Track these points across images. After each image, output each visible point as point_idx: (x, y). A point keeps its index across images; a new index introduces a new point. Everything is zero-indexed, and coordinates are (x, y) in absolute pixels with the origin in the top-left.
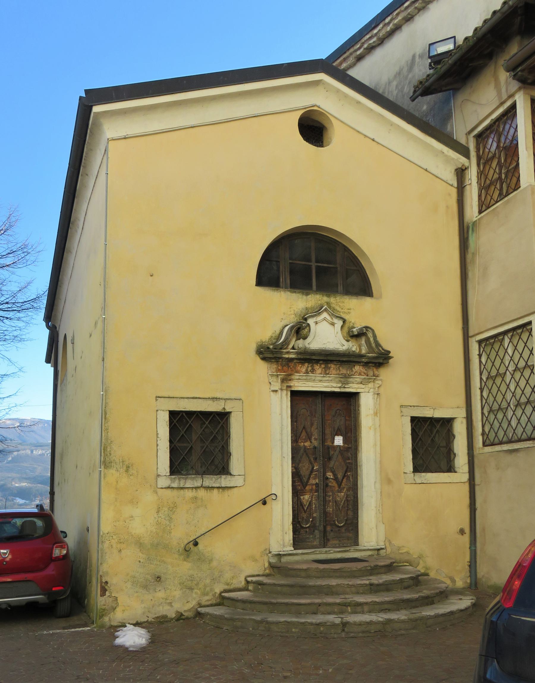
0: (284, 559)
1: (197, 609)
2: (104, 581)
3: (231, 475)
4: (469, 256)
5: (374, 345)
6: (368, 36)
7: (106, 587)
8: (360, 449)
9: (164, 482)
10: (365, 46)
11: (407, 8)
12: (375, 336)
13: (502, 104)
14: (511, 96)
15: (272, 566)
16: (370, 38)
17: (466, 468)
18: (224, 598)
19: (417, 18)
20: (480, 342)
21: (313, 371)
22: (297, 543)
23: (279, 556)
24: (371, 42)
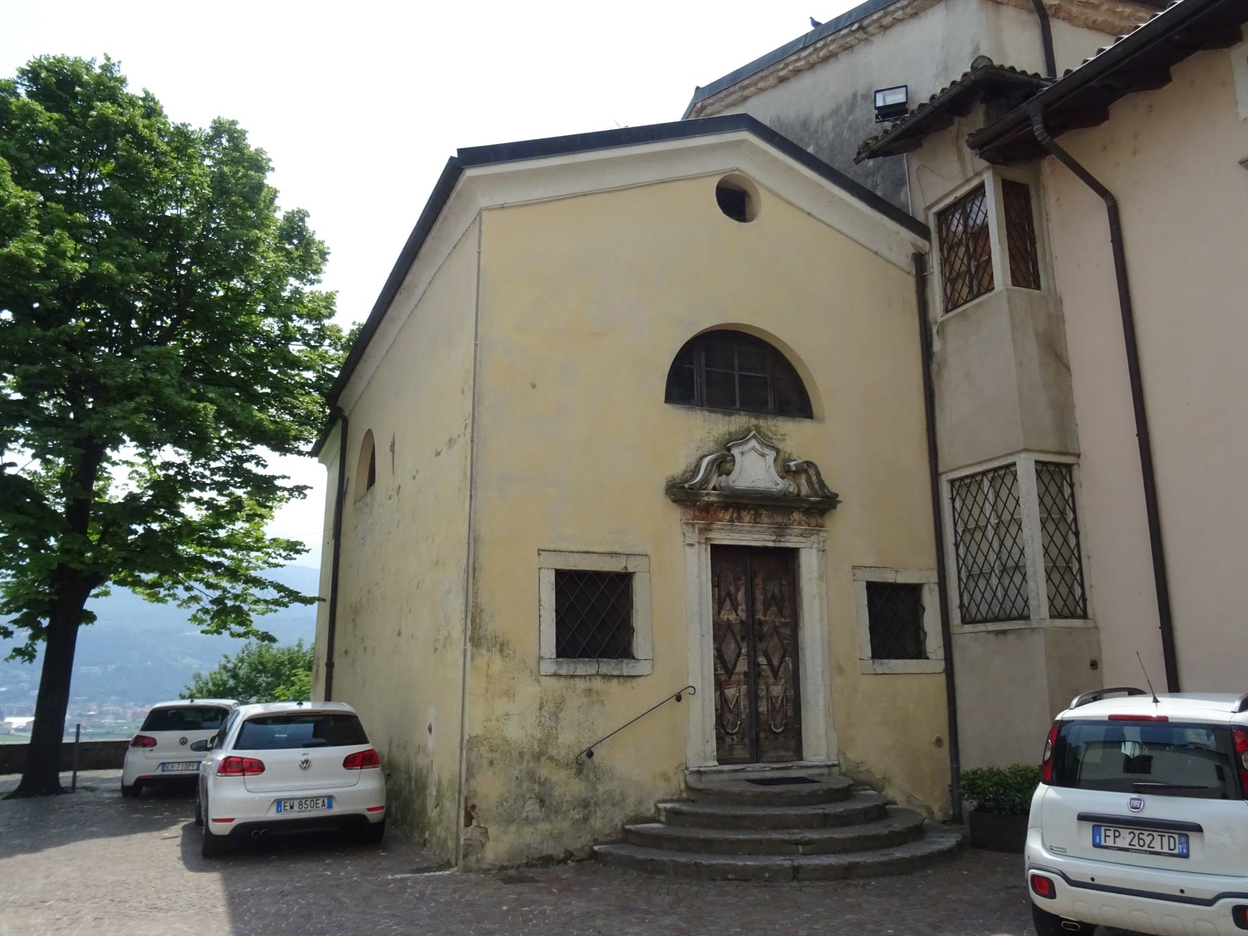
4: (934, 367)
5: (816, 486)
12: (818, 474)
13: (968, 181)
15: (689, 788)
17: (941, 653)
19: (857, 48)
20: (952, 482)
24: (799, 64)
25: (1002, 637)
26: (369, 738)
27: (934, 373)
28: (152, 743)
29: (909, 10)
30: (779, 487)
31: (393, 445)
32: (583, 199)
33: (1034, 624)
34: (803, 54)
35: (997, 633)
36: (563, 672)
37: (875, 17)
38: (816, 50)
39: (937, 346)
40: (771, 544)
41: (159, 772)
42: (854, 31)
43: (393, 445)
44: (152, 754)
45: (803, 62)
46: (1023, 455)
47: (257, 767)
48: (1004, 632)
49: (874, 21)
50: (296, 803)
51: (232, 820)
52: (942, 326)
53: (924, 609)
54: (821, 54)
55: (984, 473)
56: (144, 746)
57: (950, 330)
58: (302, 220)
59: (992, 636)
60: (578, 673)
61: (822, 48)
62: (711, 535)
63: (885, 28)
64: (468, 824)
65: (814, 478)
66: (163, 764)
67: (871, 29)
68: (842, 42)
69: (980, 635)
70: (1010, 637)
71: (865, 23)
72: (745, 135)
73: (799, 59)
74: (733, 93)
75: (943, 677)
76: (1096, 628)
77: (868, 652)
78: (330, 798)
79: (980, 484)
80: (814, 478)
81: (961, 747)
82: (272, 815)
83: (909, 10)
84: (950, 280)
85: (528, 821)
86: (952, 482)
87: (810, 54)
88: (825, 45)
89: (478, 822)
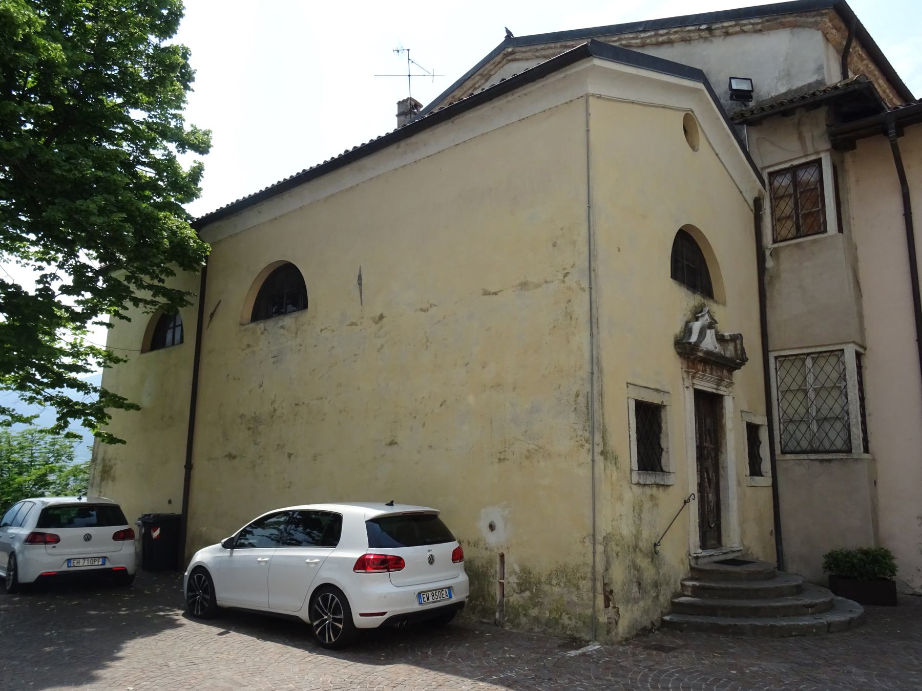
0: (700, 561)
1: (662, 619)
2: (608, 589)
3: (662, 471)
4: (767, 279)
5: (739, 352)
6: (631, 36)
7: (611, 597)
8: (723, 450)
9: (635, 478)
10: (624, 42)
11: (689, 31)
12: (742, 344)
13: (806, 156)
14: (817, 153)
15: (692, 569)
16: (633, 38)
17: (770, 474)
18: (673, 603)
19: (694, 43)
20: (776, 358)
21: (70, 274)
22: (703, 546)
23: (697, 558)
24: (633, 41)
25: (825, 464)
26: (453, 532)
27: (766, 282)
28: (56, 539)
29: (759, 27)
30: (717, 350)
31: (360, 278)
32: (662, 109)
33: (855, 456)
34: (642, 35)
35: (822, 461)
36: (641, 482)
37: (726, 24)
38: (655, 35)
39: (770, 263)
40: (710, 390)
41: (65, 568)
42: (703, 30)
43: (360, 278)
44: (55, 551)
45: (638, 41)
46: (852, 345)
47: (397, 564)
48: (829, 461)
49: (723, 27)
50: (430, 593)
51: (384, 614)
52: (775, 253)
53: (760, 443)
54: (661, 39)
55: (808, 354)
56: (46, 543)
57: (783, 255)
58: (185, 56)
59: (817, 463)
60: (648, 482)
61: (662, 35)
62: (695, 381)
63: (727, 34)
64: (607, 606)
65: (739, 346)
66: (69, 560)
67: (717, 32)
68: (683, 35)
69: (804, 462)
70: (832, 464)
71: (714, 27)
72: (701, 86)
73: (637, 38)
74: (551, 48)
75: (771, 489)
76: (874, 460)
77: (748, 473)
78: (449, 588)
79: (804, 361)
80: (739, 346)
81: (784, 535)
82: (415, 607)
83: (759, 27)
84: (777, 220)
85: (636, 601)
86: (776, 358)
87: (649, 37)
88: (666, 34)
89: (614, 604)
